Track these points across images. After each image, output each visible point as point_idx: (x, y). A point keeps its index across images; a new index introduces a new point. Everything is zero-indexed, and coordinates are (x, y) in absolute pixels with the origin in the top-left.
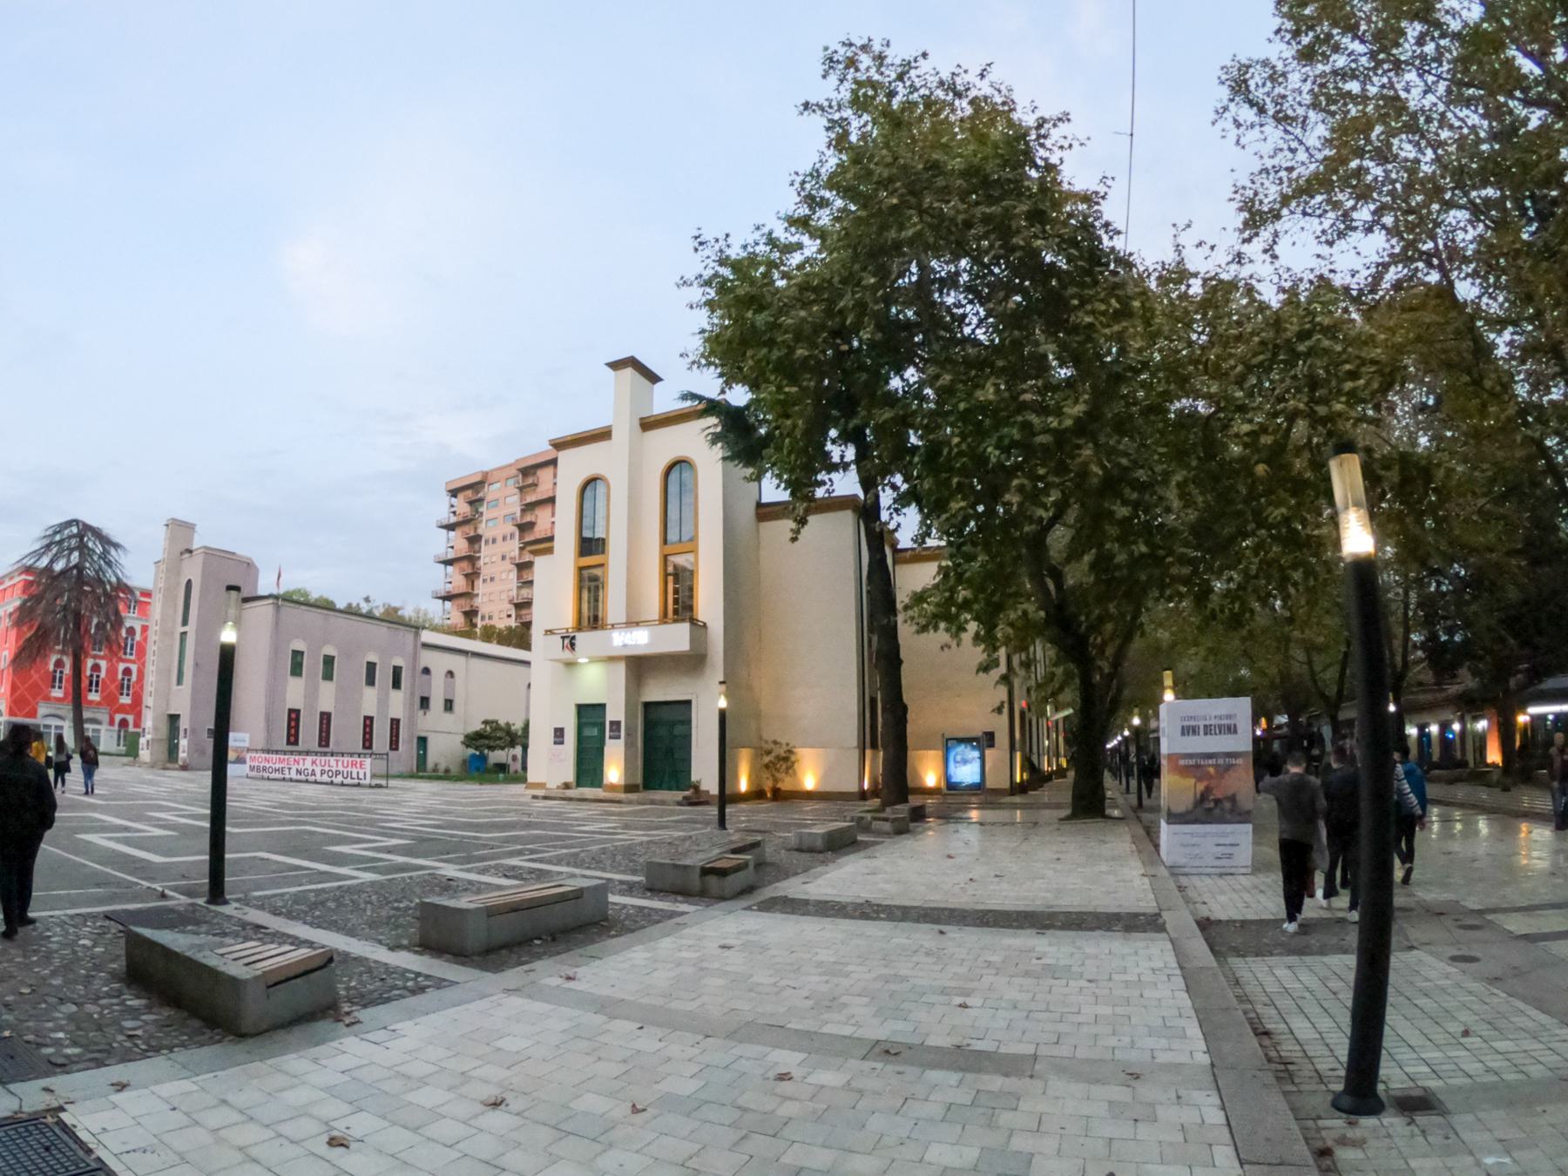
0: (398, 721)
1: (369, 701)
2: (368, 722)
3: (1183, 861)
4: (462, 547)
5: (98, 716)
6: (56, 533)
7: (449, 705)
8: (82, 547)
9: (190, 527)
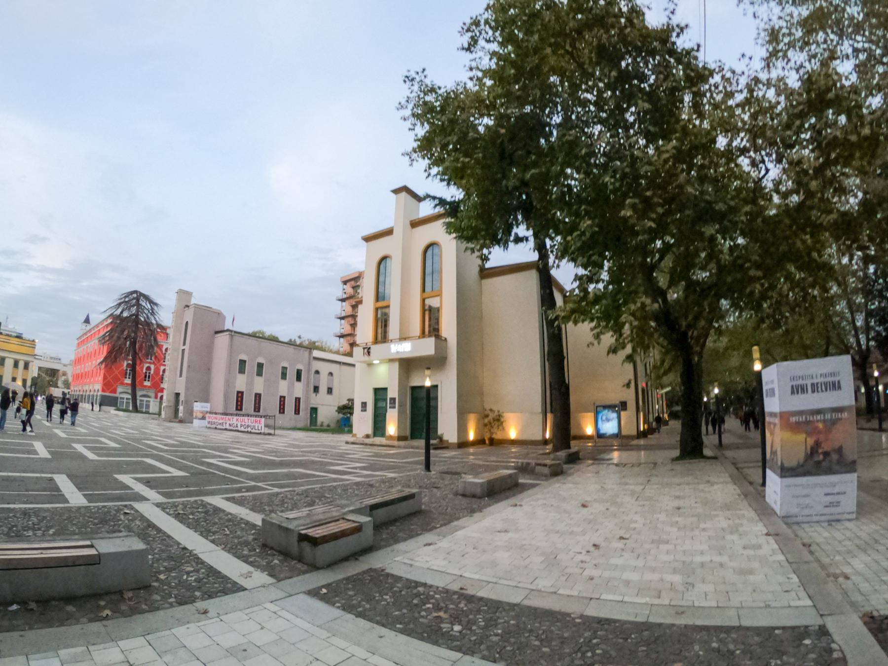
0: (299, 399)
1: (283, 388)
2: (282, 399)
3: (795, 510)
4: (349, 310)
5: (149, 394)
6: (125, 297)
7: (330, 391)
8: (138, 305)
9: (189, 294)
